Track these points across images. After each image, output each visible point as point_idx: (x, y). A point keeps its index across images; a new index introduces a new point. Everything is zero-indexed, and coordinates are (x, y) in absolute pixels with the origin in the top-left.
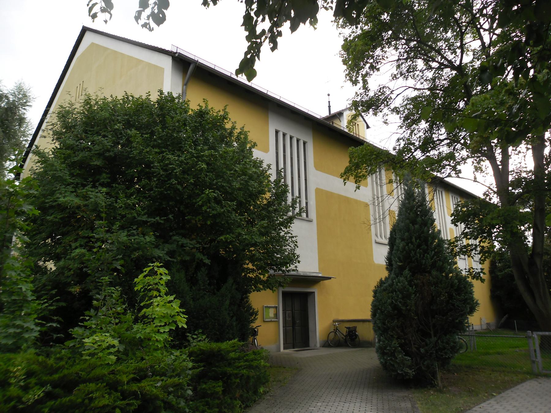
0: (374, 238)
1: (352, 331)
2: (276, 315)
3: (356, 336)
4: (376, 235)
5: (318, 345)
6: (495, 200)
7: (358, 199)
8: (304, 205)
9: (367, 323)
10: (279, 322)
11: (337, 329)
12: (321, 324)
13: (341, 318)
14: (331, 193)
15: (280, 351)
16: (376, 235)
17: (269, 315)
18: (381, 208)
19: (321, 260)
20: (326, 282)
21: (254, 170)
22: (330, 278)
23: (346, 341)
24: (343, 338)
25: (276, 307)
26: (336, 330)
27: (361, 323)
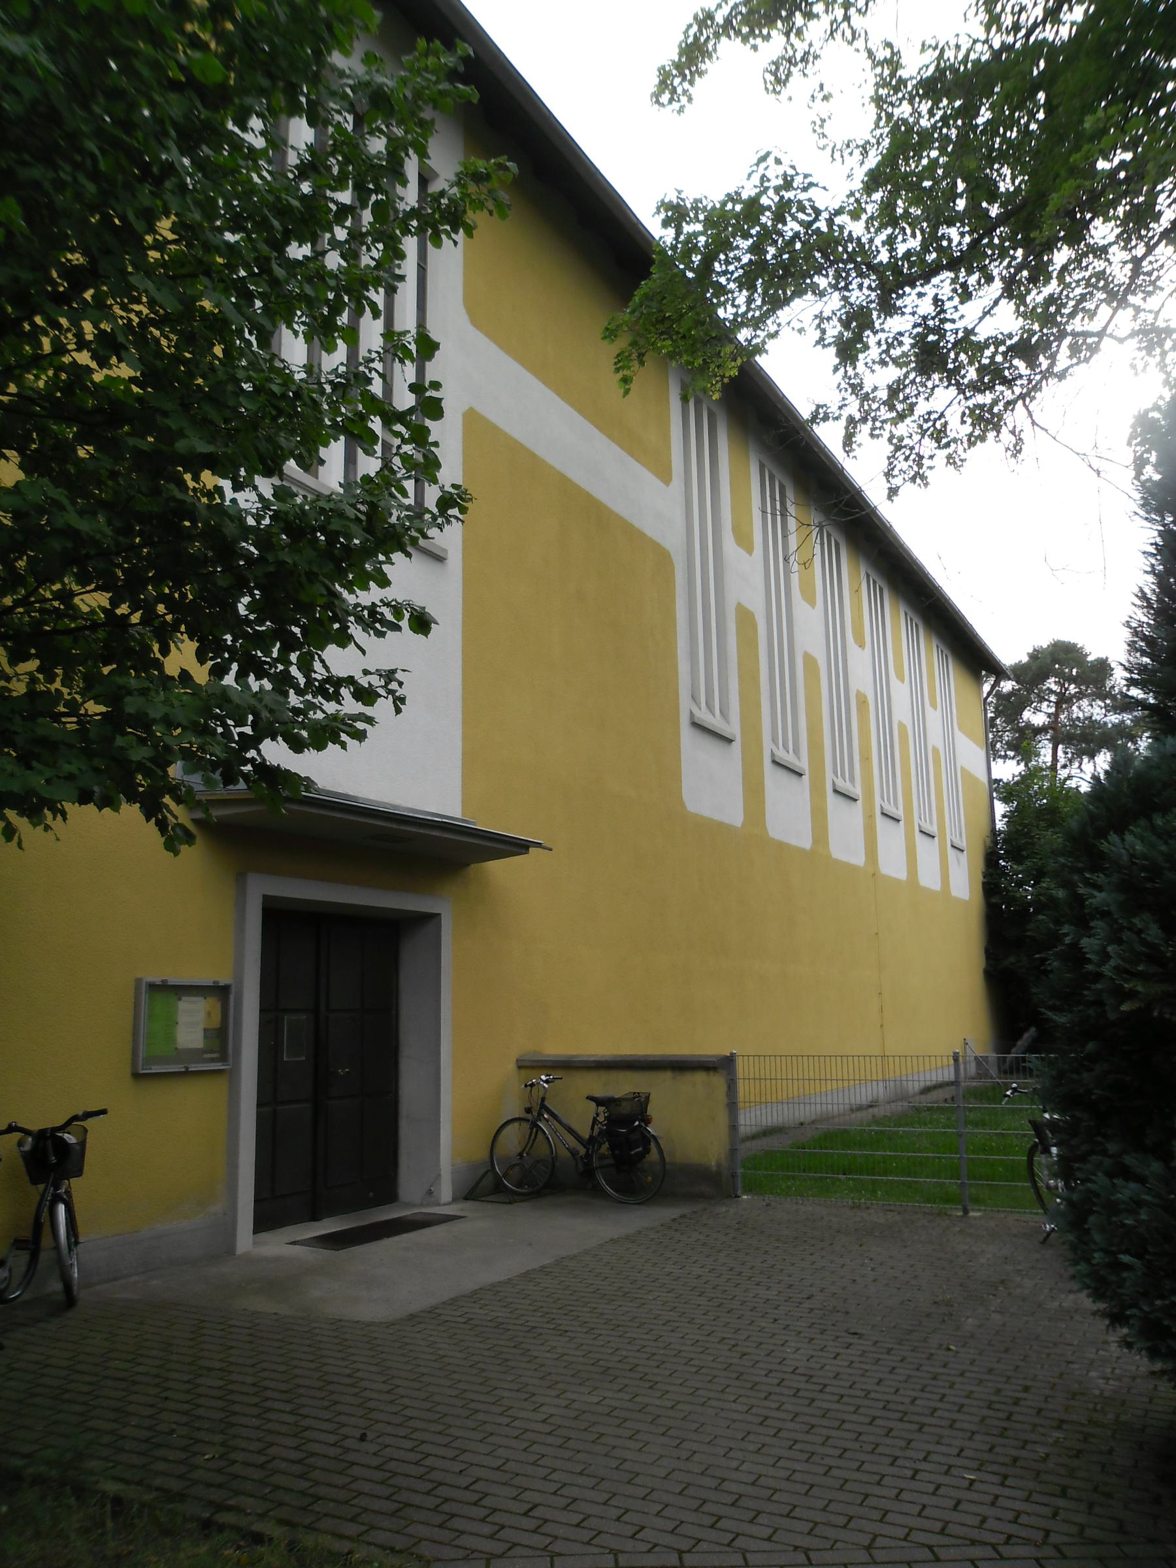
0: (685, 704)
1: (627, 1121)
2: (221, 1039)
3: (646, 1140)
4: (694, 698)
5: (446, 1192)
6: (984, 673)
7: (636, 523)
8: (406, 321)
9: (700, 1077)
10: (232, 1076)
11: (543, 1107)
12: (461, 1086)
13: (555, 1049)
14: (533, 456)
15: (230, 1250)
16: (694, 698)
17: (170, 1038)
18: (779, 518)
19: (475, 760)
20: (498, 869)
21: (73, 34)
22: (520, 847)
23: (588, 1173)
24: (574, 1153)
25: (221, 992)
26: (536, 1113)
27: (668, 1075)
